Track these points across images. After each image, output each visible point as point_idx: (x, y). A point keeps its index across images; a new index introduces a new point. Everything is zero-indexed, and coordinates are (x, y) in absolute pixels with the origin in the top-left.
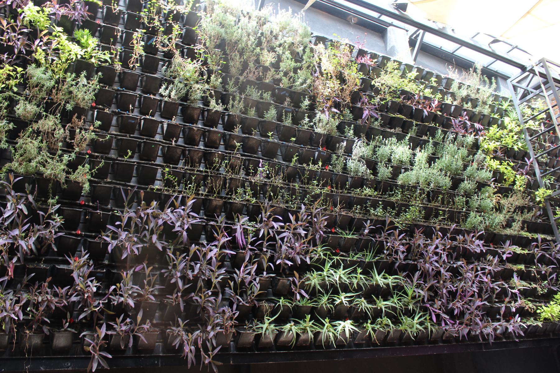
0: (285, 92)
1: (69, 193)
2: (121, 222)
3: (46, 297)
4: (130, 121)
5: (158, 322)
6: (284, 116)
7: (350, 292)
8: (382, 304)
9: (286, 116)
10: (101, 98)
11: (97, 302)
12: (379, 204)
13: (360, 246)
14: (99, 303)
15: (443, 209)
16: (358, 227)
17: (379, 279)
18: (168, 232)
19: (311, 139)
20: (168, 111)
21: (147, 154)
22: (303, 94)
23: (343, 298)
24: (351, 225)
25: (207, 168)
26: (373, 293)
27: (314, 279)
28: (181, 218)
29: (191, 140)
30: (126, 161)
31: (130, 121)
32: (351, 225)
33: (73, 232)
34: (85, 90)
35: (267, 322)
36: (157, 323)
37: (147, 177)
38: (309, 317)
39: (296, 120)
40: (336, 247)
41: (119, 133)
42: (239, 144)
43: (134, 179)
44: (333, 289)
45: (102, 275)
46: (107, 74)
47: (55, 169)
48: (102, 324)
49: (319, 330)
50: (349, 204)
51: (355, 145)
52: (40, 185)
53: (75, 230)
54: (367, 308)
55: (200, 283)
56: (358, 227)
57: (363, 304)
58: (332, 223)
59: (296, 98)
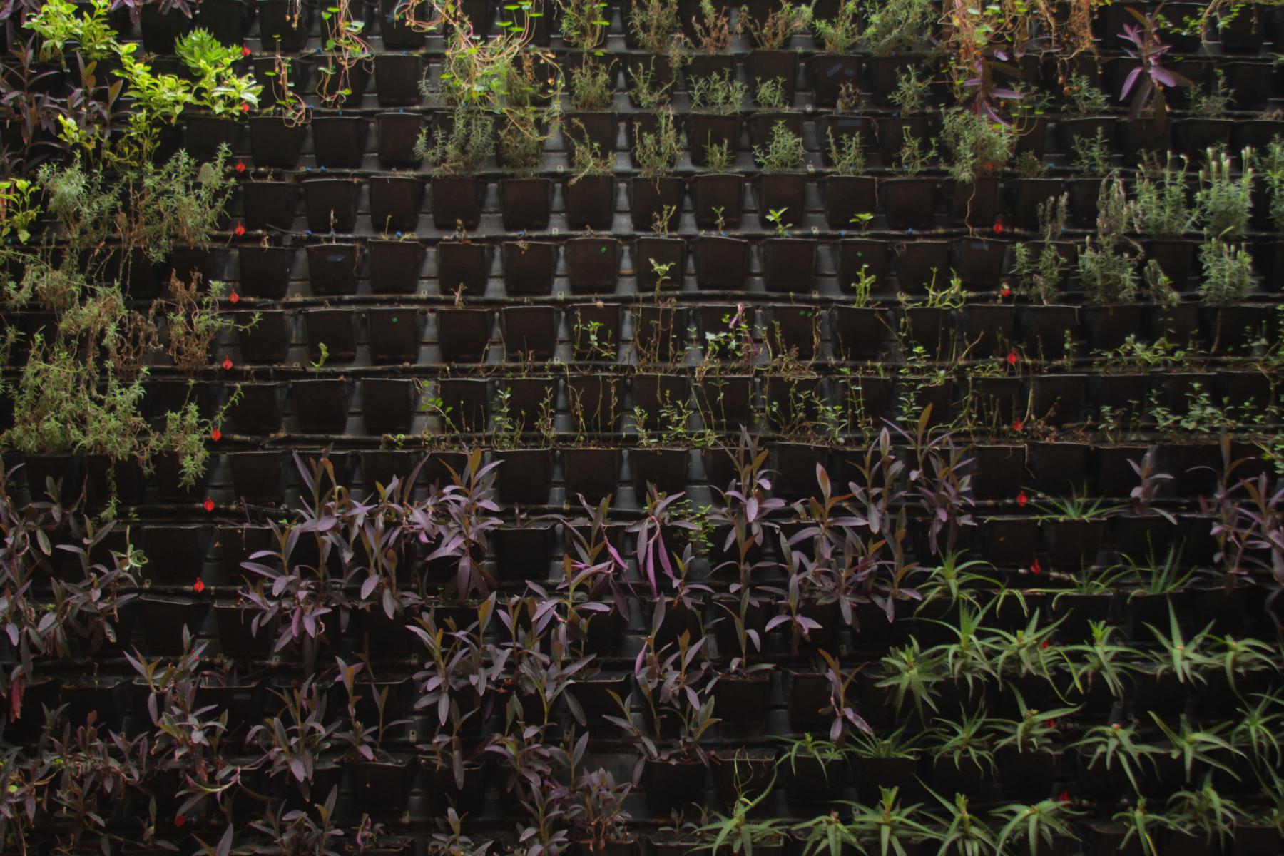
0: (838, 67)
1: (149, 487)
2: (278, 549)
3: (94, 761)
4: (330, 258)
5: (417, 819)
6: (834, 148)
7: (1058, 704)
8: (1194, 742)
9: (840, 145)
10: (244, 204)
11: (228, 769)
12: (1192, 390)
13: (1132, 540)
14: (233, 773)
15: (607, 434)
16: (1105, 475)
17: (1182, 656)
18: (413, 562)
19: (936, 200)
20: (458, 201)
21: (396, 344)
22: (902, 56)
23: (1033, 726)
24: (1067, 473)
25: (516, 359)
26: (1159, 701)
27: (908, 670)
28: (454, 519)
29: (529, 275)
30: (321, 375)
31: (330, 258)
32: (1067, 473)
33: (189, 588)
34: (190, 199)
35: (740, 811)
36: (412, 823)
37: (397, 411)
38: (890, 795)
39: (881, 147)
40: (1008, 553)
41: (308, 298)
42: (665, 268)
43: (352, 421)
44: (1001, 695)
45: (248, 697)
46: (256, 137)
47: (111, 424)
48: (221, 830)
49: (930, 834)
50: (1071, 402)
51: (1102, 196)
52: (77, 475)
53: (193, 582)
54: (1129, 757)
55: (515, 706)
56: (1105, 475)
57: (1116, 740)
58: (995, 478)
59: (875, 73)
